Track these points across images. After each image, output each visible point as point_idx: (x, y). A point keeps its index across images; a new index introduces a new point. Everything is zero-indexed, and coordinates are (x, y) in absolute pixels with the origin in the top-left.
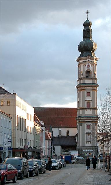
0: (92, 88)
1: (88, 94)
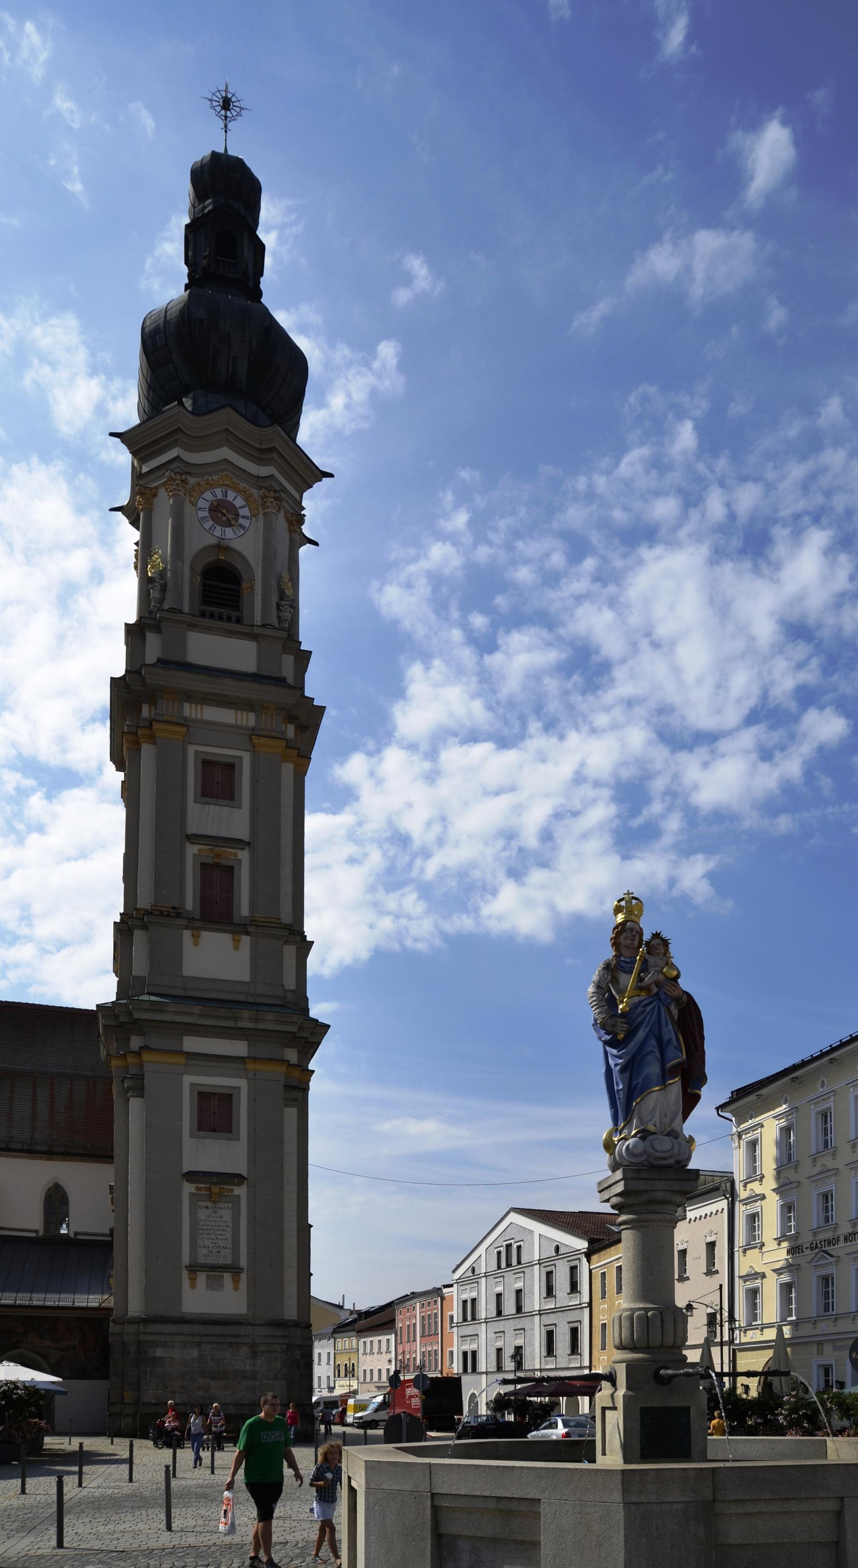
0: (250, 719)
1: (218, 782)
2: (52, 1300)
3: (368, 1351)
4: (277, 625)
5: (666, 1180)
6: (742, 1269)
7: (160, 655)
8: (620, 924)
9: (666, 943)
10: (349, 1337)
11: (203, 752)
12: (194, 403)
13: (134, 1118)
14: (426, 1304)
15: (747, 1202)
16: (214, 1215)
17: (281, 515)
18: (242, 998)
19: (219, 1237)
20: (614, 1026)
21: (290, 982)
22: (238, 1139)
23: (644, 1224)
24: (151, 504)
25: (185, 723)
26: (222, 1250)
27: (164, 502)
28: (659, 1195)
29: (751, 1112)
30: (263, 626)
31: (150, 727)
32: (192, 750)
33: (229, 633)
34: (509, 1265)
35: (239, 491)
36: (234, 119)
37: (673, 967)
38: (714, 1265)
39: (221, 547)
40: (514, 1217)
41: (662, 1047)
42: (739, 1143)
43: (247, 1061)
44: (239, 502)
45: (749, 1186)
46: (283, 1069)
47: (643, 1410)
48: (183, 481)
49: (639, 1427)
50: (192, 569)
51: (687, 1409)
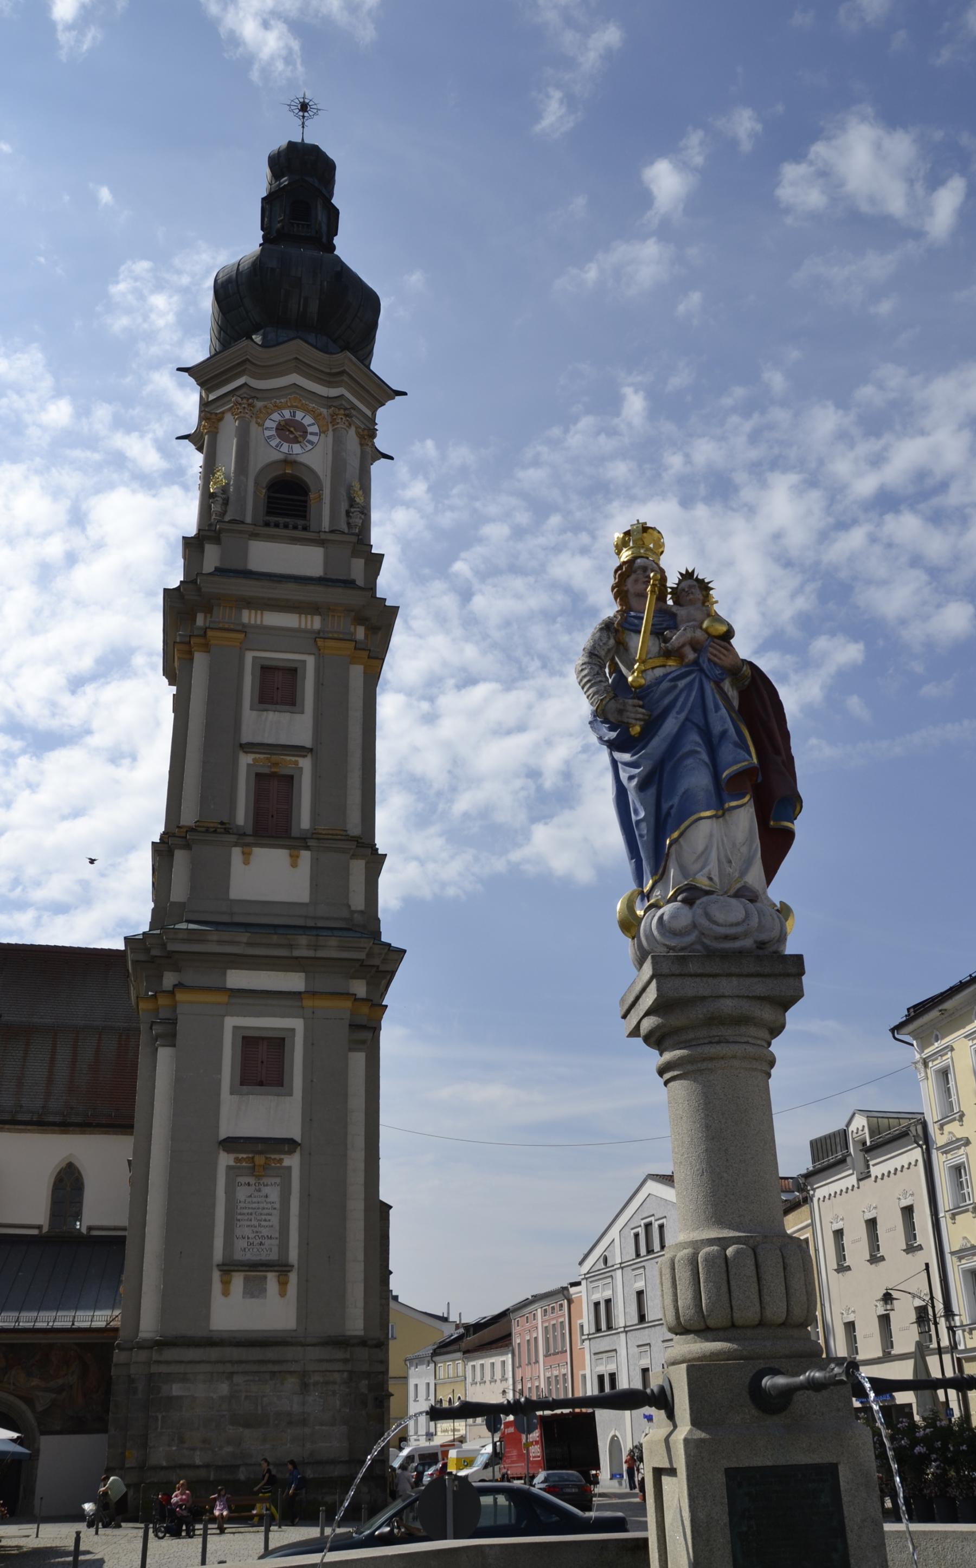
0: (316, 623)
1: (278, 688)
2: (46, 1319)
3: (478, 1379)
4: (346, 531)
5: (740, 975)
6: (952, 1242)
7: (218, 564)
8: (624, 563)
9: (704, 587)
10: (453, 1360)
11: (261, 658)
12: (263, 339)
13: (163, 1070)
14: (549, 1309)
15: (947, 1149)
16: (256, 1194)
17: (352, 431)
18: (300, 922)
19: (263, 1223)
20: (621, 712)
21: (358, 902)
22: (291, 1095)
23: (704, 1065)
24: (217, 428)
25: (244, 630)
26: (267, 1242)
27: (230, 425)
28: (728, 1006)
29: (936, 1032)
30: (332, 532)
31: (204, 635)
32: (249, 656)
33: (294, 540)
34: (650, 1251)
35: (307, 411)
36: (310, 117)
37: (718, 619)
38: (915, 1239)
39: (288, 462)
40: (653, 1187)
41: (712, 745)
42: (926, 1073)
43: (303, 996)
44: (308, 420)
45: (947, 1128)
46: (348, 1004)
47: (732, 1475)
48: (249, 405)
49: (726, 1518)
50: (256, 483)
51: (833, 1469)
